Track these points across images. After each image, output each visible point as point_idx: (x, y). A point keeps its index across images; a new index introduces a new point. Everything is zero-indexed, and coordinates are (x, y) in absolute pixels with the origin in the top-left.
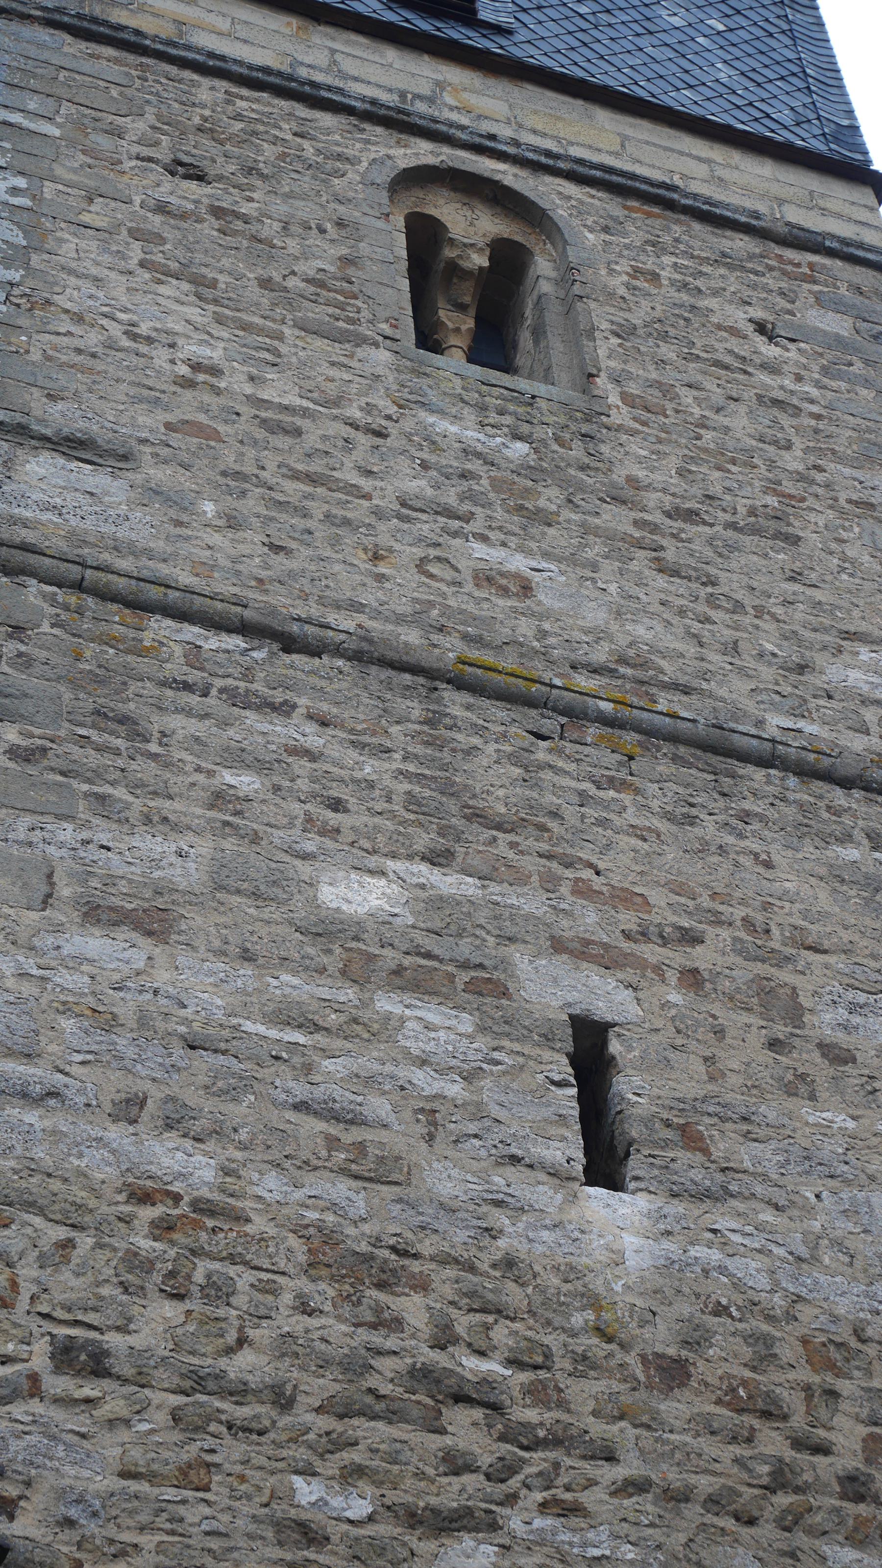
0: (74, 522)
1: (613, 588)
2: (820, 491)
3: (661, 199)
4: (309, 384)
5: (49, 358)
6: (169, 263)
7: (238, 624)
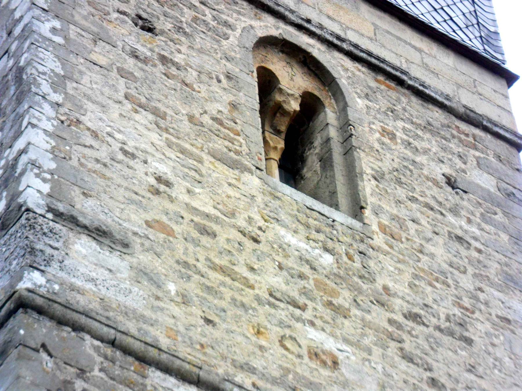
0: (104, 291)
1: (379, 368)
2: (483, 307)
3: (396, 79)
4: (218, 199)
5: (82, 164)
6: (140, 97)
7: (196, 378)
